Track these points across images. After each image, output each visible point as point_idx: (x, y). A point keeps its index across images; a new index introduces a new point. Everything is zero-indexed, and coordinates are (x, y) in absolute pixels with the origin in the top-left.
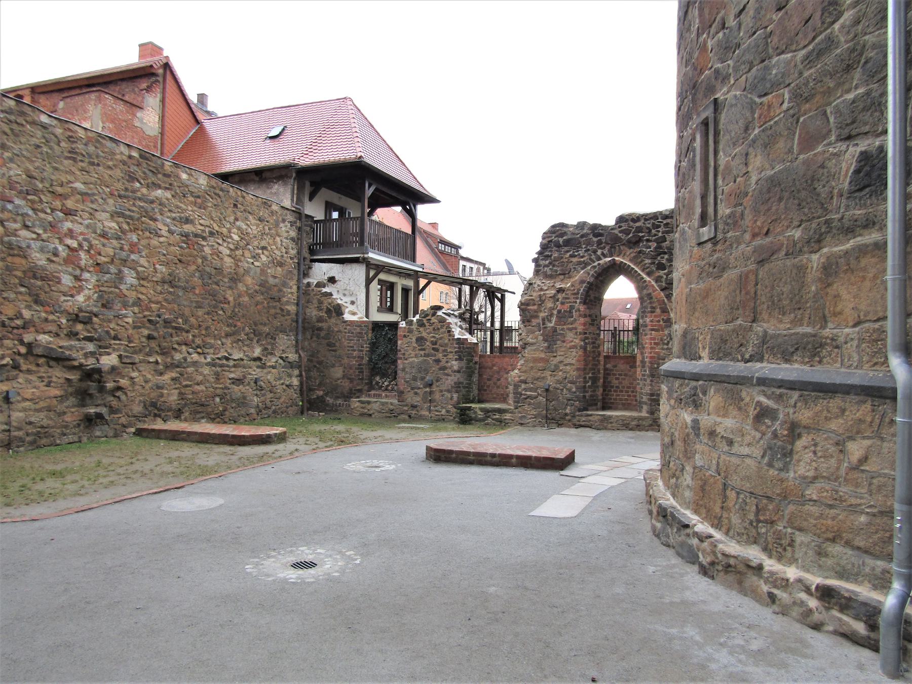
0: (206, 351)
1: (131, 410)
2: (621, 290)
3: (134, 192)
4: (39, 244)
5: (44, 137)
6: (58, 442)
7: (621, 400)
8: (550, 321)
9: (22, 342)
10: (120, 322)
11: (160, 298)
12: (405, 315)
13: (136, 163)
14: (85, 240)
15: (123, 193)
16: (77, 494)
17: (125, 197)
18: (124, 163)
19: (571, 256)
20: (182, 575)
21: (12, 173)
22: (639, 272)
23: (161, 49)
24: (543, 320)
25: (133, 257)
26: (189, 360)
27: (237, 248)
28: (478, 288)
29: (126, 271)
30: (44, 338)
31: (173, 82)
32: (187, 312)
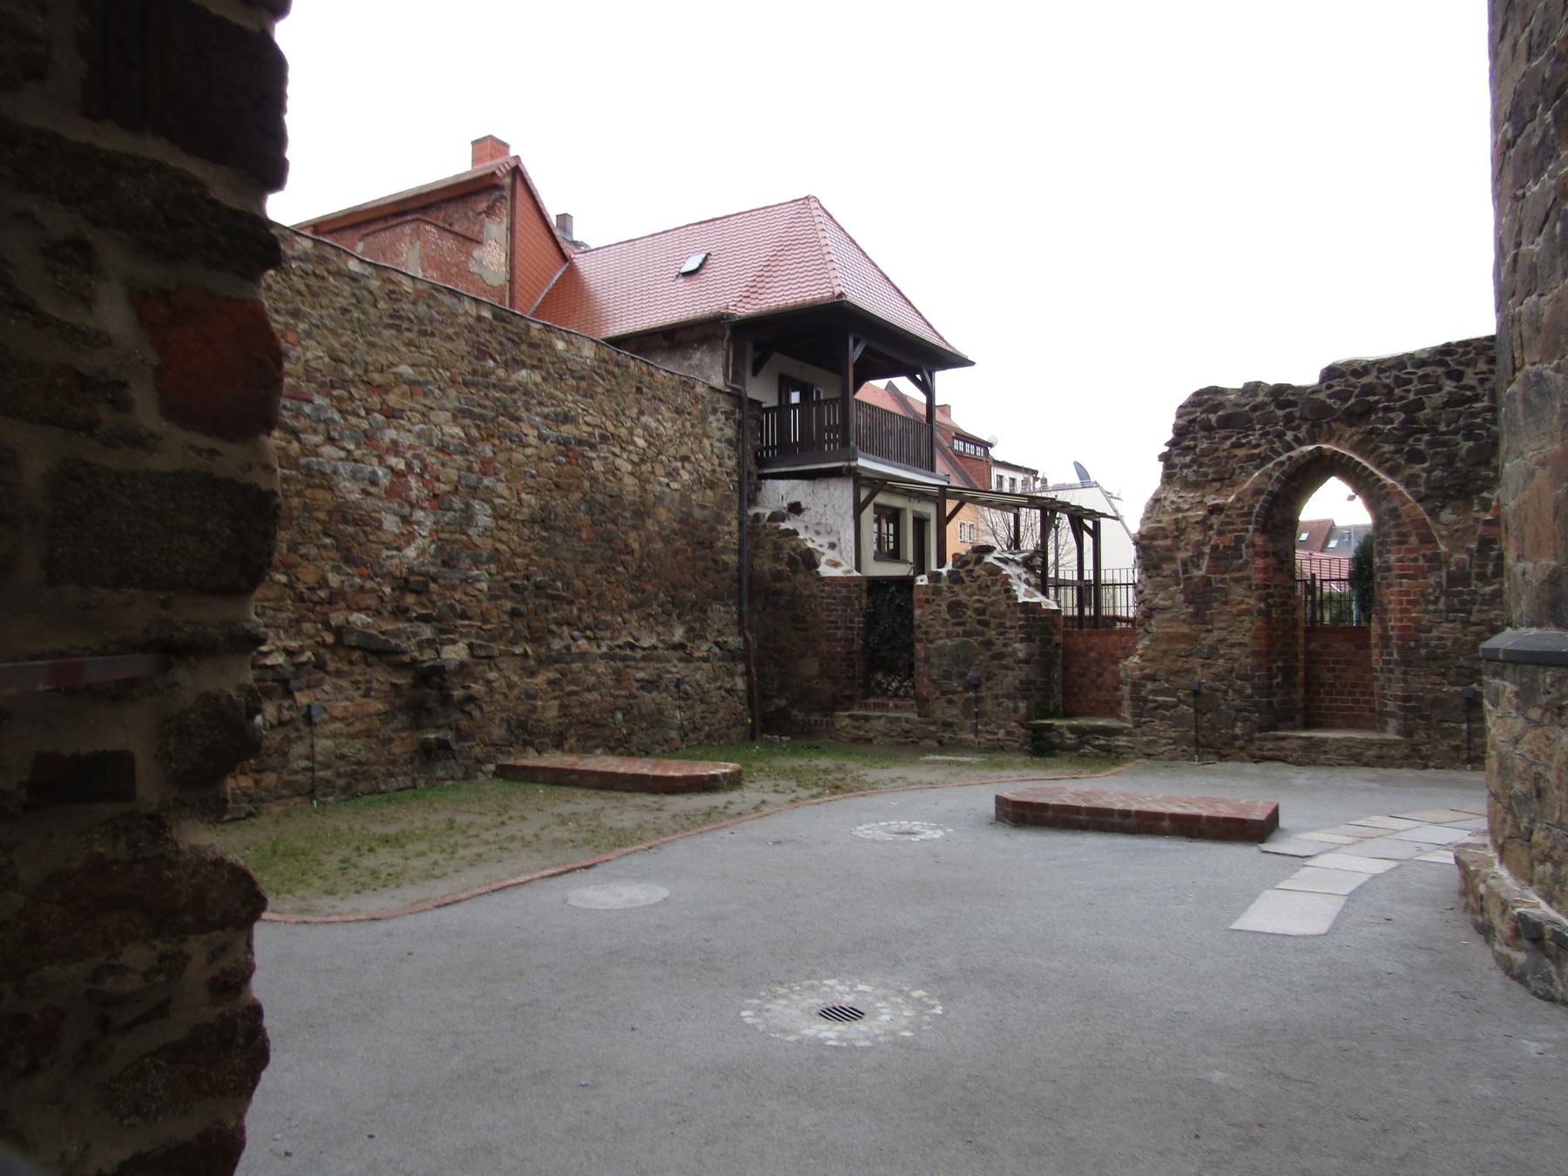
0: (600, 634)
1: (489, 734)
2: (1335, 505)
3: (486, 375)
4: (349, 466)
5: (354, 295)
6: (383, 787)
7: (1342, 709)
8: (1198, 567)
9: (327, 625)
10: (469, 590)
11: (528, 550)
12: (920, 566)
13: (487, 327)
14: (415, 456)
15: (469, 377)
16: (429, 876)
17: (474, 384)
18: (471, 329)
19: (1234, 446)
20: (637, 1025)
21: (309, 355)
22: (1372, 468)
23: (506, 146)
24: (1184, 564)
25: (487, 482)
26: (574, 649)
27: (643, 461)
28: (1054, 512)
29: (477, 505)
30: (359, 618)
31: (526, 196)
32: (569, 569)
